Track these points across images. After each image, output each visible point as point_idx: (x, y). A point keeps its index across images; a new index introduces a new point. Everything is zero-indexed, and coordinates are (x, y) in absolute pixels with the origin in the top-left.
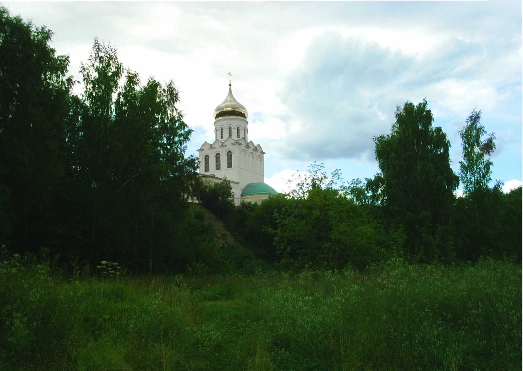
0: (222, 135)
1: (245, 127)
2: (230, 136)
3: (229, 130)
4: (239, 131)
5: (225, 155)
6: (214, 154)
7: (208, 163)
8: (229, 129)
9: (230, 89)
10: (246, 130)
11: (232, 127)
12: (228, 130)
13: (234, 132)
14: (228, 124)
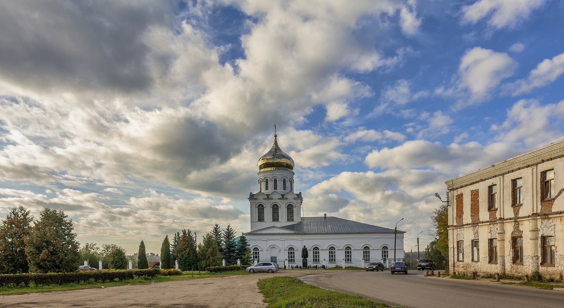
0: (266, 186)
1: (292, 178)
2: (275, 188)
3: (275, 182)
4: (285, 183)
5: (270, 208)
6: (271, 204)
8: (275, 181)
11: (278, 179)
12: (273, 182)
13: (280, 184)
14: (283, 176)
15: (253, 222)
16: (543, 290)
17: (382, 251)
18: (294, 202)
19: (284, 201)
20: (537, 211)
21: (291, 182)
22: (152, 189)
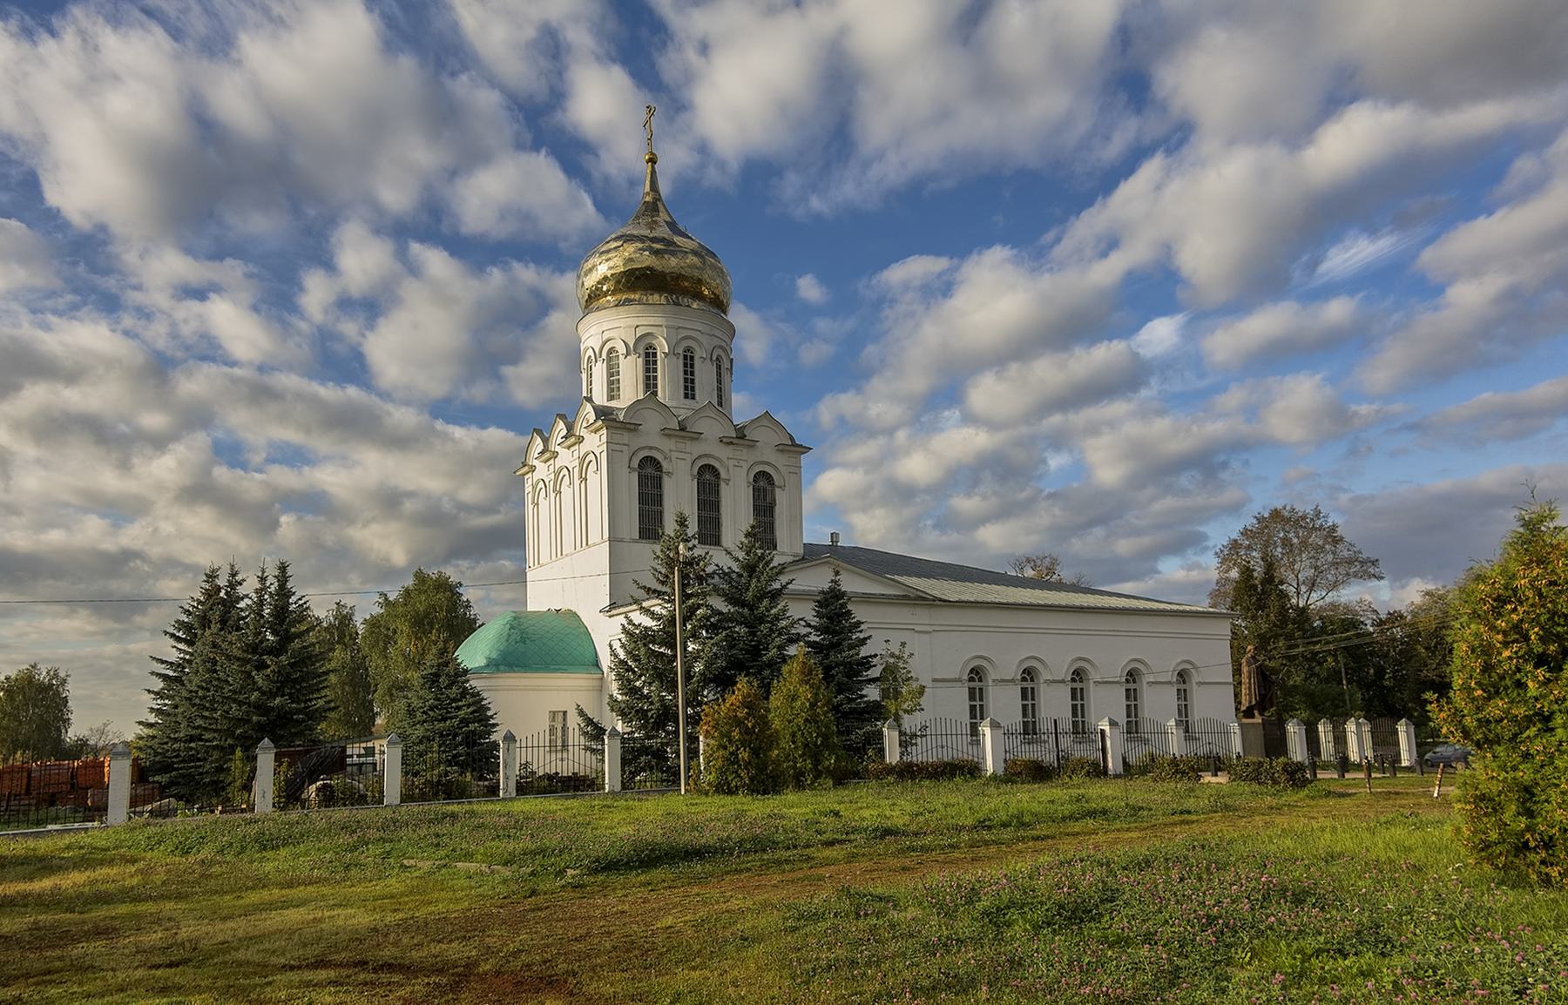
1: (721, 347)
4: (692, 366)
7: (716, 506)
9: (653, 172)
10: (726, 364)
15: (621, 541)
18: (778, 465)
19: (743, 453)
21: (719, 367)
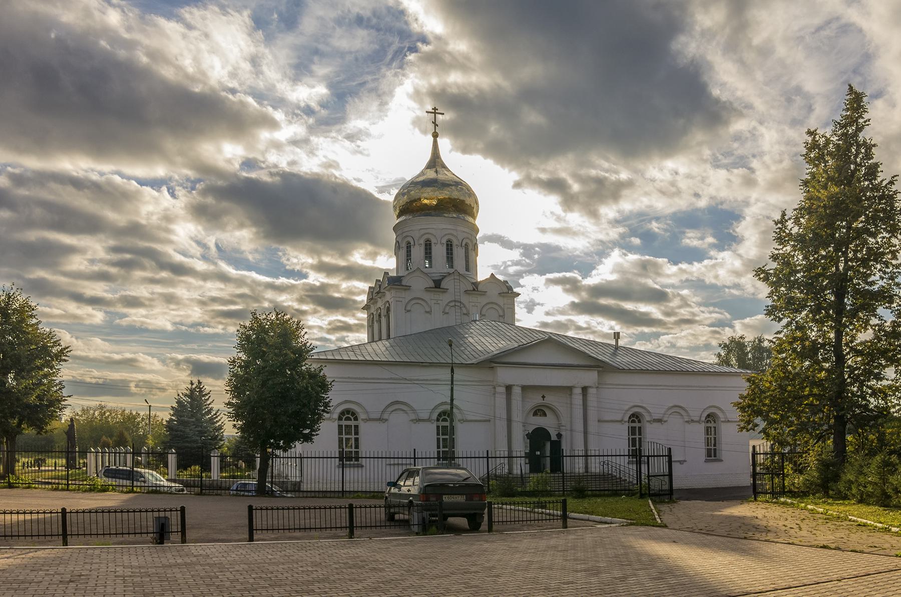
3: (426, 249)
8: (426, 245)
11: (433, 241)
12: (423, 248)
13: (439, 251)
16: (578, 514)
17: (438, 427)
20: (446, 381)
22: (314, 285)
